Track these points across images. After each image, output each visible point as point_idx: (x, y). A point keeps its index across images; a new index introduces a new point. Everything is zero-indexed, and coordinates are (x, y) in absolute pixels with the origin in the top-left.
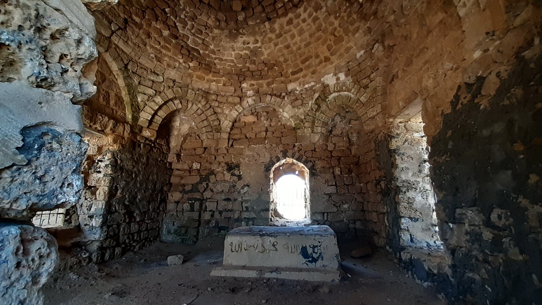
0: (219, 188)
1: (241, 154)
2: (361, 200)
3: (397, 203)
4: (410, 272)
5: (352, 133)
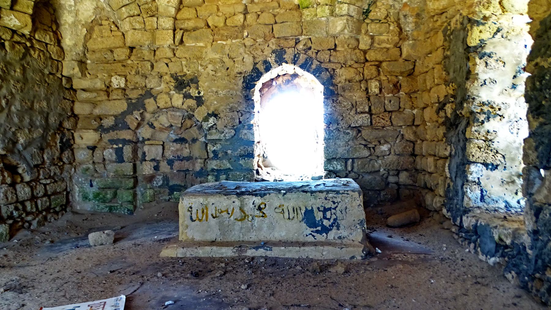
0: (164, 120)
1: (199, 58)
2: (412, 138)
3: (467, 140)
4: (472, 245)
5: (405, 16)
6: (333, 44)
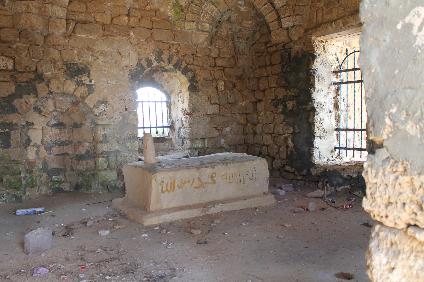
6: (195, 50)
